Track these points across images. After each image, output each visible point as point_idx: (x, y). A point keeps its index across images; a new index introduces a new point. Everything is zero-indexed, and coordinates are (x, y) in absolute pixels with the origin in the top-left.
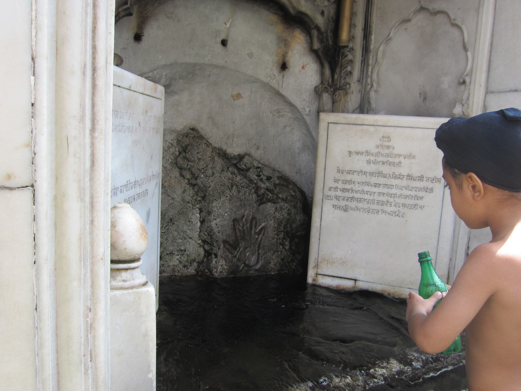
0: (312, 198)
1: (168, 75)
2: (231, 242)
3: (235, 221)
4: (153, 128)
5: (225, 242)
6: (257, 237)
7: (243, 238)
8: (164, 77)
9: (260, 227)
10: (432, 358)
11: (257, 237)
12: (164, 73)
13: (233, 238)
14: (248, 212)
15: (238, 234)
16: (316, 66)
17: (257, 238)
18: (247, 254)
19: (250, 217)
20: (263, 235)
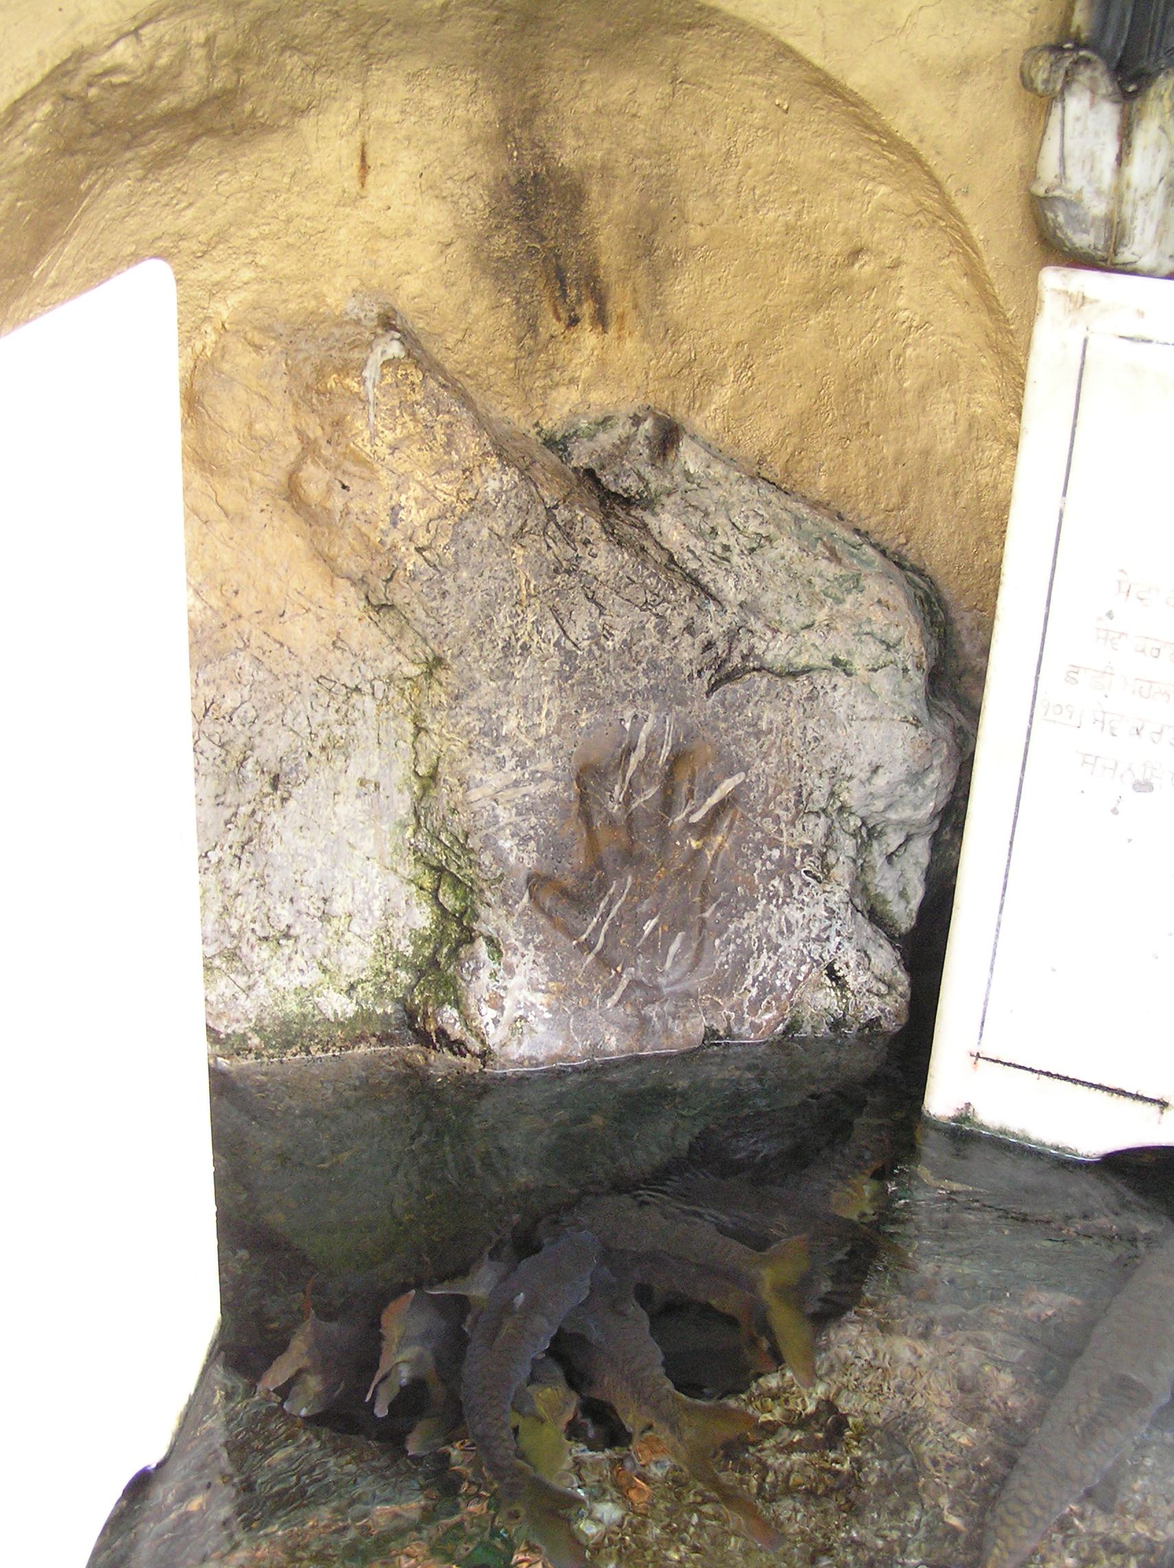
0: (985, 627)
1: (221, 40)
2: (569, 882)
3: (589, 778)
4: (793, 1026)
5: (536, 882)
6: (694, 844)
7: (630, 857)
8: (199, 53)
9: (713, 800)
10: (259, 1030)
11: (694, 844)
12: (199, 36)
13: (580, 860)
14: (651, 726)
15: (603, 836)
16: (932, 1112)
17: (698, 853)
18: (649, 926)
19: (665, 752)
20: (692, 782)
